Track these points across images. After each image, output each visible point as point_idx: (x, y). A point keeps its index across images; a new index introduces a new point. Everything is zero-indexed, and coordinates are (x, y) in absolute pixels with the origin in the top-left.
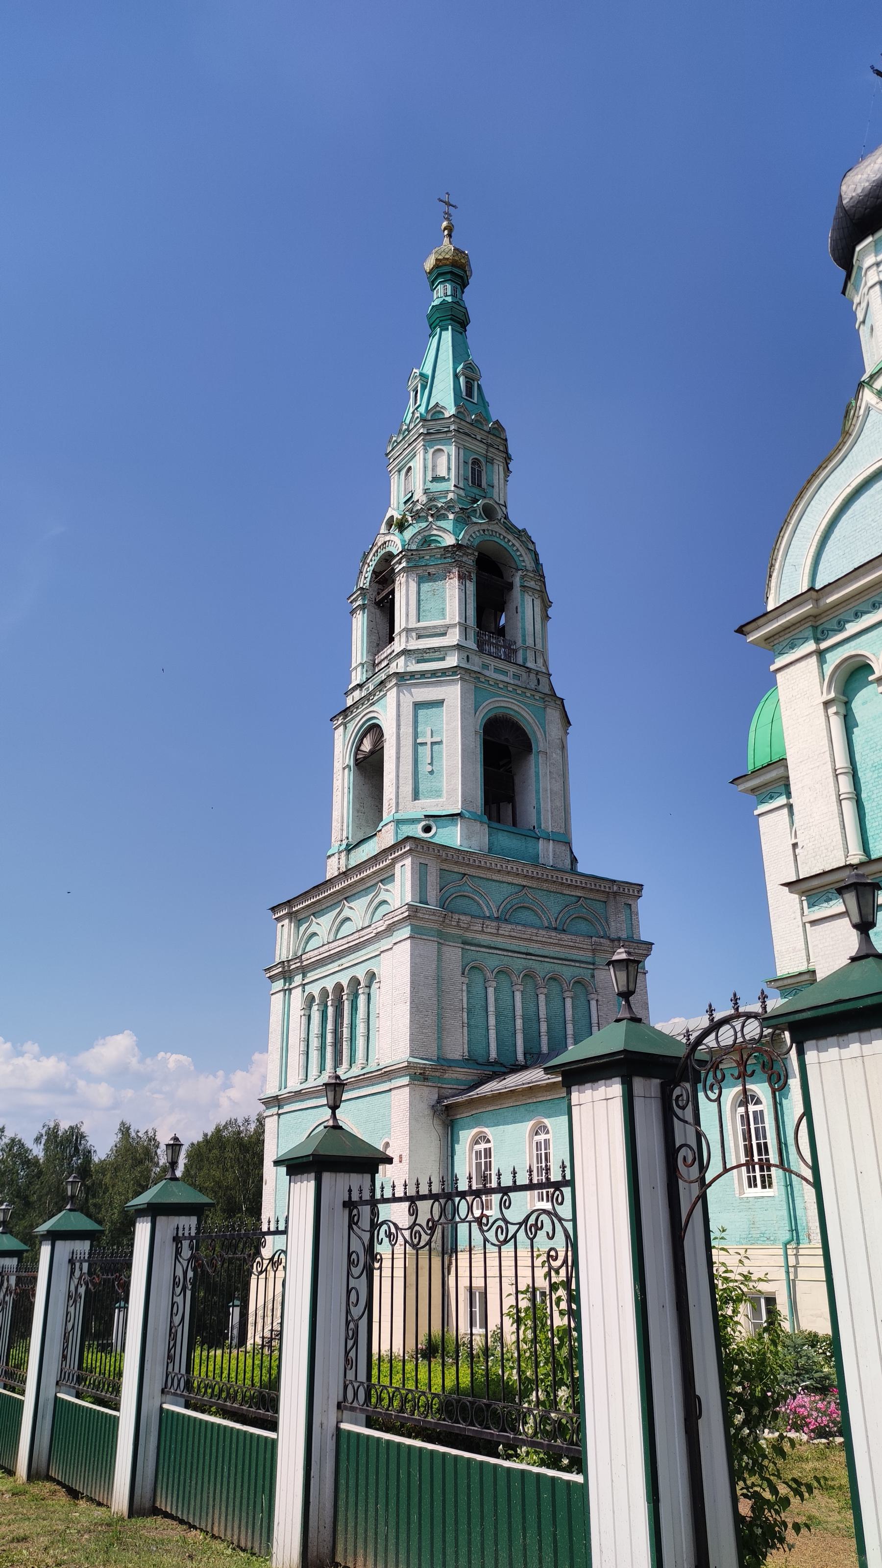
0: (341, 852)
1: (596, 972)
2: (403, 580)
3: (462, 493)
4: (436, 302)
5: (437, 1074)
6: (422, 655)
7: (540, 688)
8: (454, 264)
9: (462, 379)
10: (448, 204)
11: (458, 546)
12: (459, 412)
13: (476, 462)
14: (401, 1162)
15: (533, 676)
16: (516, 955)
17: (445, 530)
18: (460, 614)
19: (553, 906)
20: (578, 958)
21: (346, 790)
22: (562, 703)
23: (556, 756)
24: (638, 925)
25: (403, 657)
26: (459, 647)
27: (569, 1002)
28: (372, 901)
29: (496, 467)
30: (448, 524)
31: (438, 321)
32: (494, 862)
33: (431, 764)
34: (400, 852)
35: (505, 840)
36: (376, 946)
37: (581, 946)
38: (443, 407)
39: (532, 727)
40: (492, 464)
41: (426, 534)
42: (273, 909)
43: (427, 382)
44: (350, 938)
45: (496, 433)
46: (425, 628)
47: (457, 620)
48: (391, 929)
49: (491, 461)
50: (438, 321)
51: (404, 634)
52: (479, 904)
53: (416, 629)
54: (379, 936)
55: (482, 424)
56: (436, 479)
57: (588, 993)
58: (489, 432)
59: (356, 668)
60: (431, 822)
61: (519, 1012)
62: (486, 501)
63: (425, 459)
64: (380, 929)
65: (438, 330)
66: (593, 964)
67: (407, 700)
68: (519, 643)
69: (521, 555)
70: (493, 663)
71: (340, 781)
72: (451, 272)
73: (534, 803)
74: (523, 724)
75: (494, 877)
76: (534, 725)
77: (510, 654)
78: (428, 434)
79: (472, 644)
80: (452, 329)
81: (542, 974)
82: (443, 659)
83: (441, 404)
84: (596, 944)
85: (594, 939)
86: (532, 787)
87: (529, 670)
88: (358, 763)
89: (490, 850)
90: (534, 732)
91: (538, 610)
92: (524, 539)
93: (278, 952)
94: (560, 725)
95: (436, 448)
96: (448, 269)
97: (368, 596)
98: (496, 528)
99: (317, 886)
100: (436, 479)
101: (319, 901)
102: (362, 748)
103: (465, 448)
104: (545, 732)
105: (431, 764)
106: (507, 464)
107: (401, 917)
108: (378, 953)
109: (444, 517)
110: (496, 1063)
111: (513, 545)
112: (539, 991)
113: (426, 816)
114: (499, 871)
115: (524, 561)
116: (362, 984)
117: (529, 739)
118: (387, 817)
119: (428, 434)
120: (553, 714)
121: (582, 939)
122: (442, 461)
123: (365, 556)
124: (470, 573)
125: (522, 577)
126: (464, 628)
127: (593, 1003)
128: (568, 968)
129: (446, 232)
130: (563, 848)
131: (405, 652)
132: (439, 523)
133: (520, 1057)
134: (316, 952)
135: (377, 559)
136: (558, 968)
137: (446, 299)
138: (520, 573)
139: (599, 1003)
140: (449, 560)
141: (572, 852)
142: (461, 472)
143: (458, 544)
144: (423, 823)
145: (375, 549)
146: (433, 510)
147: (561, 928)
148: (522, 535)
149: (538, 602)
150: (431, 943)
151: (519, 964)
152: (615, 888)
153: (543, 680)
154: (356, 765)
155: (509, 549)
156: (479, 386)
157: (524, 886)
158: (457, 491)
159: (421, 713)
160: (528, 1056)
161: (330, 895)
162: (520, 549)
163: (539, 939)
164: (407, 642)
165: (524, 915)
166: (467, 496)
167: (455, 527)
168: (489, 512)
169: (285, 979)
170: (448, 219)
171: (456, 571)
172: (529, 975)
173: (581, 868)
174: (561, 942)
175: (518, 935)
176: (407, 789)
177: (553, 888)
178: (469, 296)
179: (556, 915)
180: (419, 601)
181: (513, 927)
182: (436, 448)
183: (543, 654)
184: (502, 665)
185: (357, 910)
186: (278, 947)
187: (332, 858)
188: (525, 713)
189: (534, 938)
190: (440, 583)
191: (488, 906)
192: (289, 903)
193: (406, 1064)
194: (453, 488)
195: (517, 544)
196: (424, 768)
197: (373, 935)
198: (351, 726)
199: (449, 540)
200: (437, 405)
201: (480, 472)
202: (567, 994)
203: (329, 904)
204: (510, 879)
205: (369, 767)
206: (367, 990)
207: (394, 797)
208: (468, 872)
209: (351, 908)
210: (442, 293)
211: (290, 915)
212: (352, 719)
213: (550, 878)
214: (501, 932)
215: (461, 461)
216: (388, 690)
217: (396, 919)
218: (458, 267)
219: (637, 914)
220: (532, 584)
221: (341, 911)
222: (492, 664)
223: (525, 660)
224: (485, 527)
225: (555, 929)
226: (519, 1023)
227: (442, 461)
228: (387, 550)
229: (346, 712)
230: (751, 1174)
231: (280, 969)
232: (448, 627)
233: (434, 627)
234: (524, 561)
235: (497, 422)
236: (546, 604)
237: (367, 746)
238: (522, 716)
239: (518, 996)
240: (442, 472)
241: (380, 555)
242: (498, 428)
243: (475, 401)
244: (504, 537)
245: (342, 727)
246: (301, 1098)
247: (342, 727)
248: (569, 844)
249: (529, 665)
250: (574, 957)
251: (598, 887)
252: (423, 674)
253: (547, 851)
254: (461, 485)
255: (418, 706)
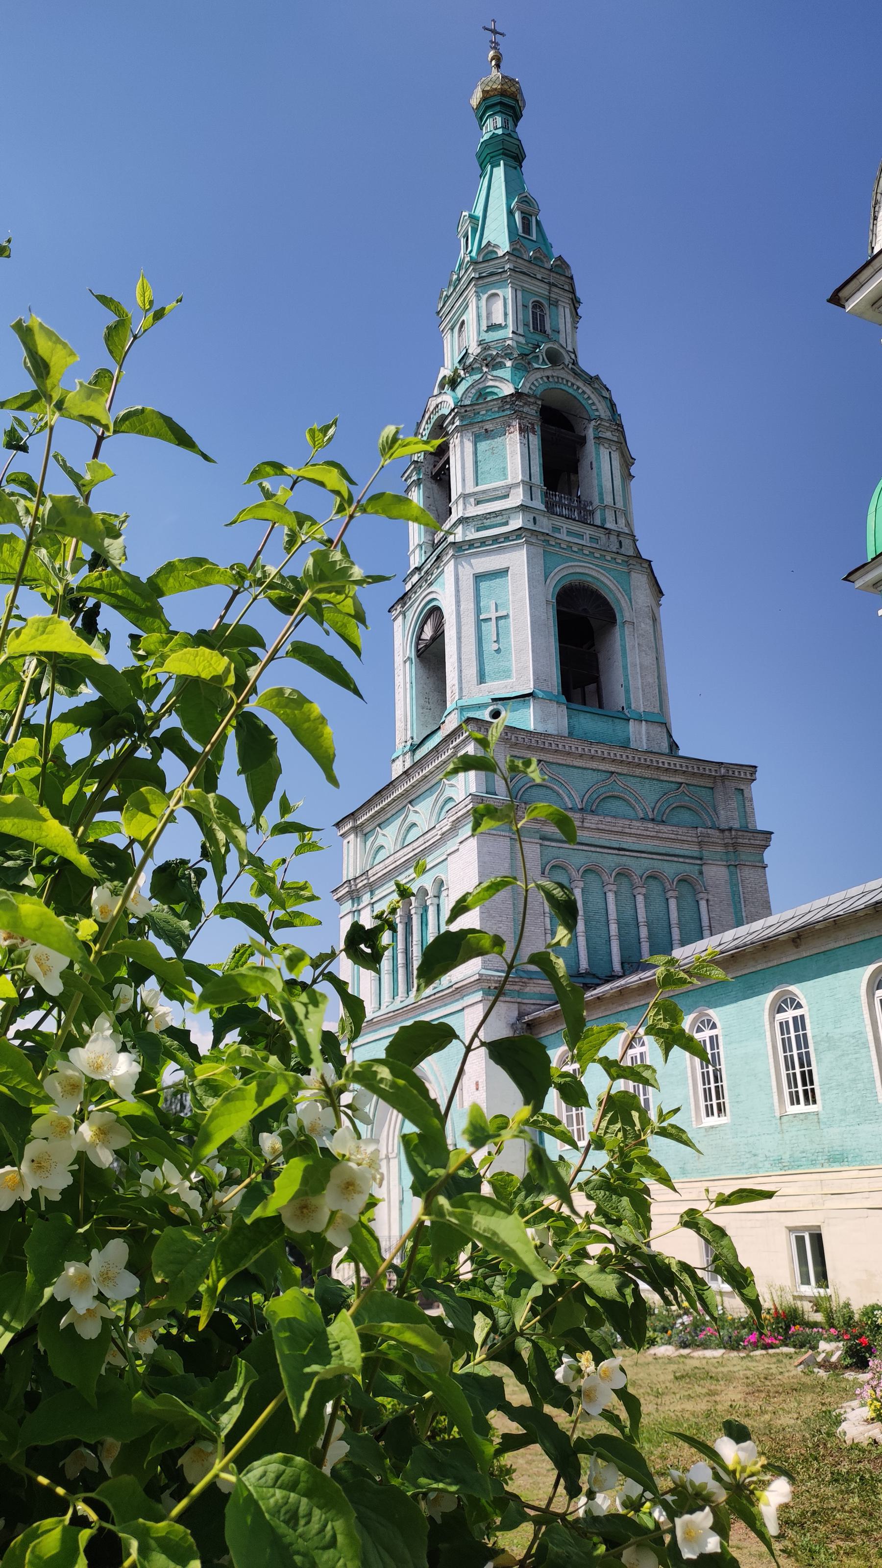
0: (405, 754)
1: (705, 868)
2: (457, 441)
3: (522, 340)
4: (486, 137)
5: (517, 988)
6: (481, 522)
7: (623, 551)
8: (503, 93)
9: (517, 216)
10: (495, 32)
11: (518, 395)
12: (514, 250)
13: (537, 305)
14: (803, 1087)
15: (613, 538)
16: (606, 851)
17: (502, 379)
18: (523, 472)
19: (648, 794)
20: (682, 853)
21: (408, 686)
22: (650, 565)
23: (646, 626)
24: (753, 813)
25: (461, 527)
26: (523, 508)
27: (673, 903)
28: (436, 801)
29: (561, 309)
30: (506, 373)
31: (488, 158)
32: (573, 746)
33: (497, 641)
34: (461, 738)
35: (589, 723)
36: (443, 849)
37: (685, 838)
38: (496, 246)
39: (614, 595)
40: (557, 306)
41: (481, 386)
42: (338, 825)
43: (478, 224)
44: (415, 845)
45: (560, 271)
46: (484, 492)
47: (520, 478)
48: (455, 826)
49: (555, 304)
50: (488, 158)
51: (461, 501)
52: (558, 794)
53: (474, 494)
54: (445, 837)
55: (542, 261)
56: (492, 328)
57: (695, 893)
58: (551, 270)
59: (413, 551)
60: (499, 706)
61: (613, 915)
62: (550, 345)
63: (478, 307)
64: (444, 829)
65: (489, 167)
66: (701, 859)
67: (467, 572)
68: (596, 502)
69: (593, 404)
70: (565, 525)
71: (402, 676)
72: (501, 103)
73: (622, 681)
74: (604, 592)
75: (576, 764)
76: (616, 592)
77: (584, 513)
78: (480, 278)
79: (538, 504)
80: (505, 164)
81: (639, 872)
82: (506, 523)
83: (493, 242)
84: (702, 835)
85: (699, 829)
86: (618, 656)
87: (609, 531)
88: (420, 654)
89: (571, 734)
90: (618, 601)
91: (616, 464)
92: (596, 386)
93: (345, 872)
94: (648, 591)
95: (490, 293)
96: (497, 99)
97: (423, 469)
98: (563, 374)
99: (379, 792)
100: (492, 328)
101: (383, 809)
102: (424, 636)
103: (524, 290)
104: (630, 600)
105: (497, 641)
106: (576, 309)
107: (465, 810)
108: (444, 857)
109: (501, 365)
110: (587, 974)
111: (584, 392)
112: (635, 892)
113: (494, 700)
114: (581, 755)
115: (597, 410)
116: (430, 894)
117: (612, 609)
118: (450, 706)
119: (480, 278)
120: (639, 580)
121: (685, 830)
122: (498, 307)
123: (419, 425)
124: (533, 424)
125: (596, 428)
126: (529, 487)
127: (703, 904)
128: (670, 864)
129: (493, 63)
130: (659, 731)
131: (462, 521)
132: (495, 373)
133: (617, 967)
134: (382, 865)
135: (430, 426)
136: (658, 865)
137: (497, 132)
138: (593, 423)
139: (711, 903)
140: (508, 412)
141: (671, 736)
142: (520, 316)
143: (517, 392)
144: (491, 708)
145: (427, 416)
146: (489, 360)
147: (659, 819)
148: (593, 381)
149: (616, 456)
150: (501, 839)
151: (610, 861)
152: (723, 771)
153: (627, 542)
154: (418, 656)
155: (580, 398)
156: (538, 223)
157: (613, 773)
158: (516, 337)
159: (483, 585)
160: (626, 966)
161: (394, 800)
162: (592, 396)
163: (633, 831)
164: (465, 509)
165: (614, 806)
166: (527, 344)
167: (513, 375)
168: (553, 358)
169: (353, 899)
170: (495, 48)
171: (516, 423)
172: (623, 874)
173: (681, 753)
174: (660, 835)
175: (607, 828)
176: (471, 672)
177: (647, 773)
178: (523, 130)
179: (652, 805)
180: (476, 463)
181: (601, 818)
182: (490, 293)
183: (625, 513)
184: (576, 527)
185: (422, 814)
186: (345, 866)
187: (397, 762)
188: (605, 579)
189: (627, 830)
190: (499, 440)
191: (570, 796)
192: (352, 815)
193: (477, 977)
194: (511, 335)
195: (588, 391)
196: (490, 647)
197: (438, 837)
198: (410, 614)
199: (507, 390)
200: (489, 244)
201: (542, 317)
202: (670, 894)
203: (394, 812)
204: (594, 765)
205: (431, 656)
206: (436, 900)
207: (456, 683)
208: (544, 758)
209: (416, 812)
210: (493, 125)
211: (355, 829)
212: (411, 606)
213: (642, 761)
214: (586, 825)
215: (520, 303)
216: (445, 565)
217: (460, 814)
218: (509, 97)
219: (751, 800)
220: (608, 435)
221: (407, 816)
222: (565, 526)
223: (604, 520)
224: (549, 373)
225: (653, 820)
226: (614, 928)
227: (498, 307)
228: (440, 413)
229: (403, 599)
230: (809, 1087)
231: (347, 889)
232: (510, 487)
233: (495, 489)
234: (597, 410)
235: (560, 258)
236: (627, 461)
237: (428, 633)
238: (602, 582)
239: (611, 897)
240: (498, 319)
241: (433, 421)
242: (562, 265)
243: (534, 238)
244: (573, 384)
245: (401, 617)
246: (374, 1028)
247: (401, 617)
248: (665, 725)
249: (608, 526)
250: (677, 852)
251: (701, 771)
252: (483, 542)
253: (639, 735)
254: (521, 331)
255: (479, 578)
